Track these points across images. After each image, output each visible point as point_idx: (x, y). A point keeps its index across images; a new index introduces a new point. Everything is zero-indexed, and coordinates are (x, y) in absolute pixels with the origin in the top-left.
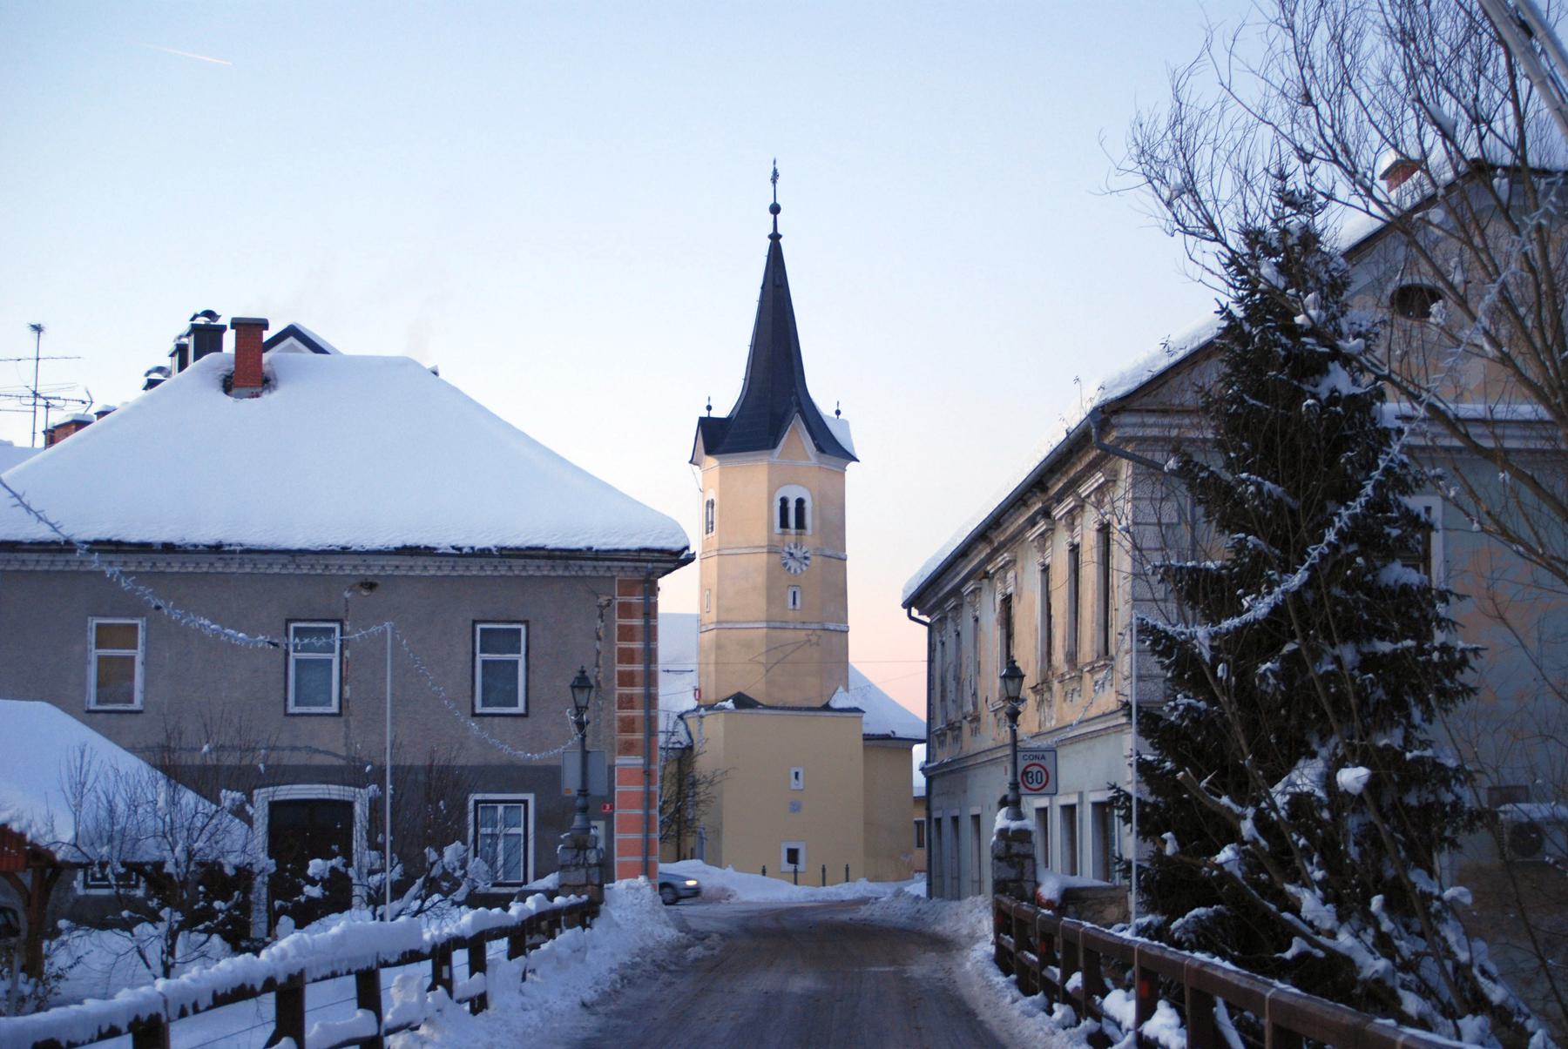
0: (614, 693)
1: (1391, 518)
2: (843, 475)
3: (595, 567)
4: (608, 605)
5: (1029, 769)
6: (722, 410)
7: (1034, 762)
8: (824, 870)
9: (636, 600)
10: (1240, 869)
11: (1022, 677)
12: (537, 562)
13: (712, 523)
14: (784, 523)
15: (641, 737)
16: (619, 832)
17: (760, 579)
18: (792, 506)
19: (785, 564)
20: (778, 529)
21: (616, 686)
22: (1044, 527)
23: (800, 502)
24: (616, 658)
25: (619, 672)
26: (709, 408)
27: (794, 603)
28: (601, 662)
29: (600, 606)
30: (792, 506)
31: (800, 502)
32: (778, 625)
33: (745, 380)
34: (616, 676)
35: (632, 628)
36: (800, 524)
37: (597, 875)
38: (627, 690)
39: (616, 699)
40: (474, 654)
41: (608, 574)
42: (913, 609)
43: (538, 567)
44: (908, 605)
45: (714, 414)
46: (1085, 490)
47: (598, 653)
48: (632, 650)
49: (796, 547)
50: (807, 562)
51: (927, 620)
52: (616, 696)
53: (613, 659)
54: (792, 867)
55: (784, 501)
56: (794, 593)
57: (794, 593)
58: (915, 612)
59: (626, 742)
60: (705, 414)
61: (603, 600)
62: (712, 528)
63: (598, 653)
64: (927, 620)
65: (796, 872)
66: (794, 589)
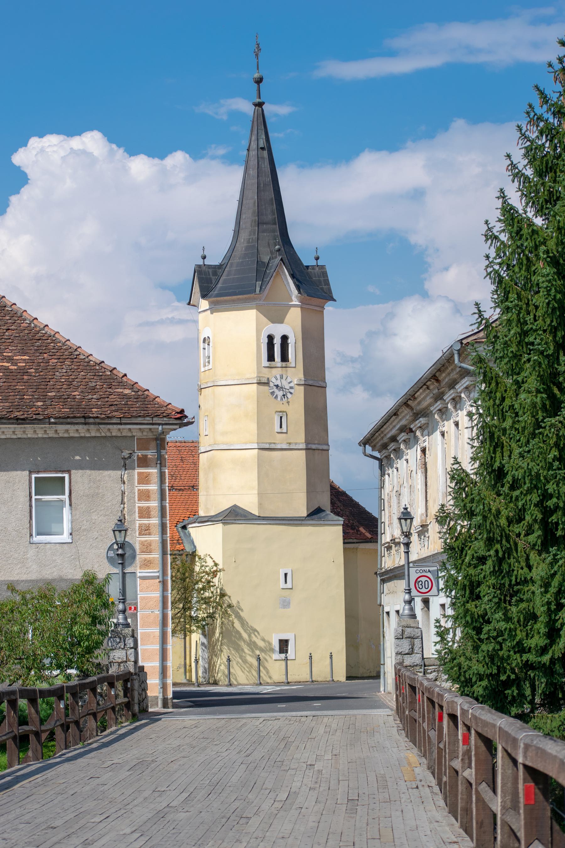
0: (135, 523)
1: (11, 713)
2: (322, 312)
3: (119, 430)
4: (130, 457)
5: (419, 580)
6: (214, 260)
7: (423, 574)
8: (311, 657)
9: (151, 454)
10: (442, 634)
11: (412, 519)
12: (77, 427)
13: (209, 357)
14: (271, 358)
15: (157, 556)
16: (142, 626)
17: (252, 407)
18: (277, 342)
19: (273, 393)
20: (265, 363)
21: (137, 518)
22: (440, 406)
23: (285, 338)
24: (136, 497)
25: (139, 507)
26: (204, 258)
27: (281, 427)
28: (126, 500)
29: (124, 459)
30: (277, 342)
31: (285, 338)
32: (267, 446)
33: (235, 231)
34: (137, 510)
35: (148, 475)
36: (285, 358)
37: (133, 655)
38: (145, 521)
39: (137, 528)
40: (31, 497)
41: (130, 434)
42: (367, 446)
43: (77, 430)
44: (365, 442)
45: (207, 262)
46: (460, 387)
47: (123, 493)
48: (148, 491)
49: (282, 377)
50: (292, 391)
51: (377, 454)
52: (137, 525)
53: (134, 497)
54: (283, 656)
55: (271, 338)
56: (281, 418)
57: (281, 418)
58: (369, 449)
59: (145, 560)
60: (201, 262)
61: (126, 454)
62: (209, 362)
63: (123, 493)
64: (377, 454)
65: (286, 659)
66: (281, 414)
